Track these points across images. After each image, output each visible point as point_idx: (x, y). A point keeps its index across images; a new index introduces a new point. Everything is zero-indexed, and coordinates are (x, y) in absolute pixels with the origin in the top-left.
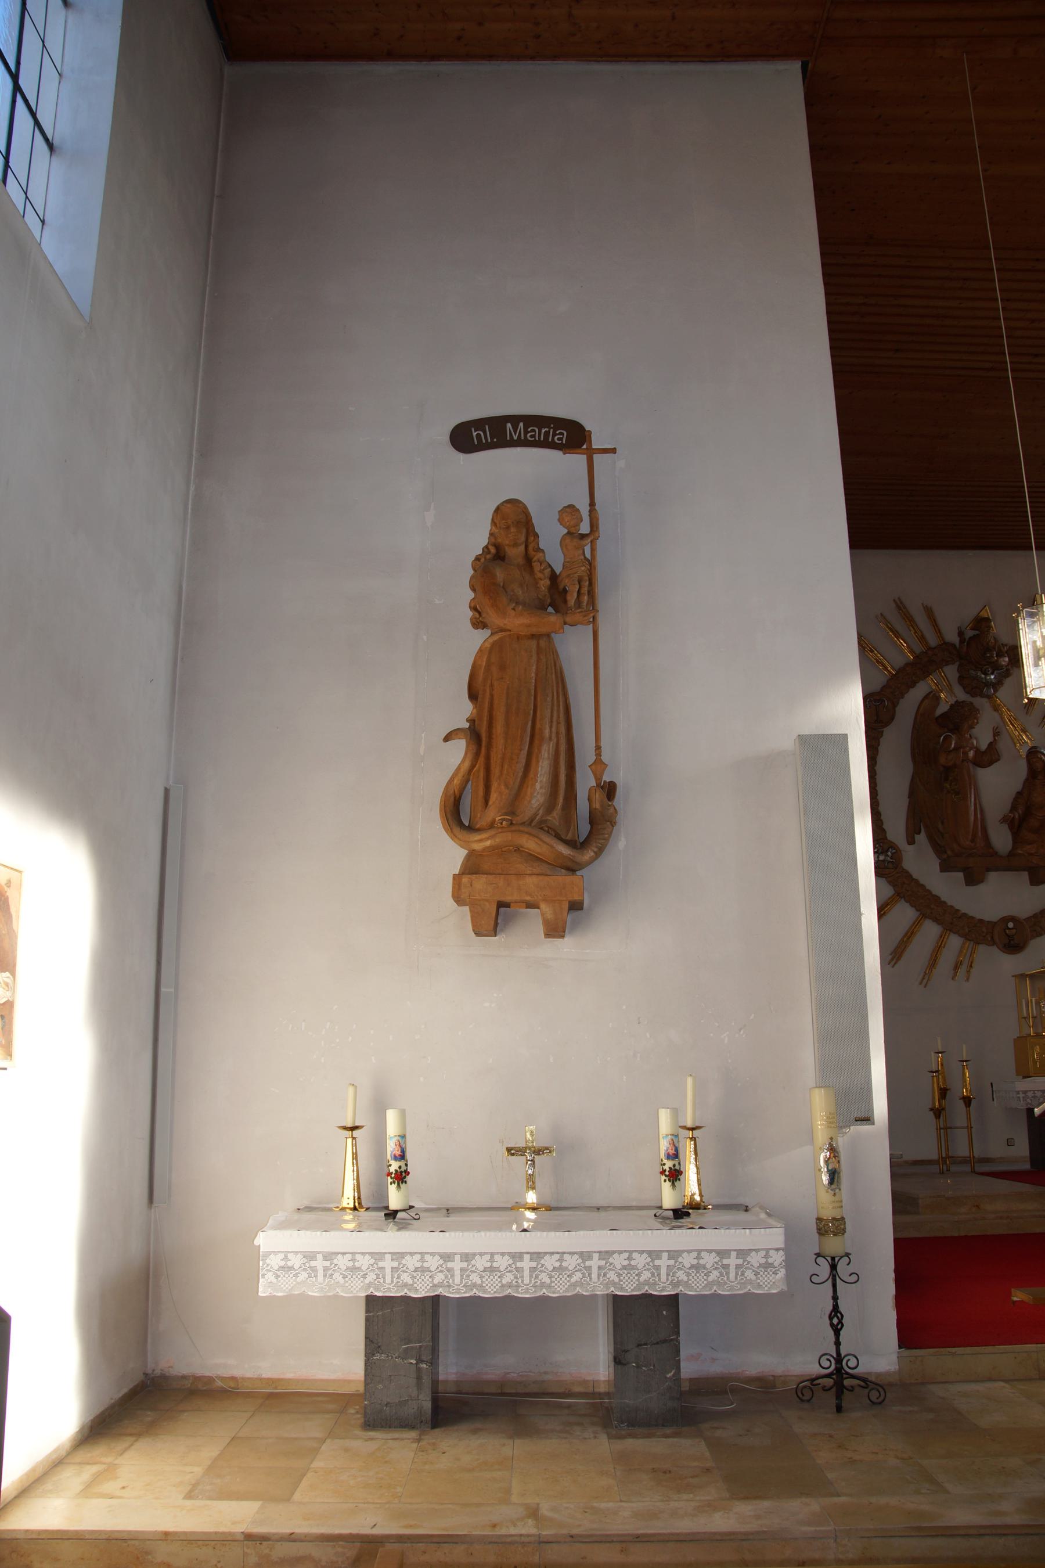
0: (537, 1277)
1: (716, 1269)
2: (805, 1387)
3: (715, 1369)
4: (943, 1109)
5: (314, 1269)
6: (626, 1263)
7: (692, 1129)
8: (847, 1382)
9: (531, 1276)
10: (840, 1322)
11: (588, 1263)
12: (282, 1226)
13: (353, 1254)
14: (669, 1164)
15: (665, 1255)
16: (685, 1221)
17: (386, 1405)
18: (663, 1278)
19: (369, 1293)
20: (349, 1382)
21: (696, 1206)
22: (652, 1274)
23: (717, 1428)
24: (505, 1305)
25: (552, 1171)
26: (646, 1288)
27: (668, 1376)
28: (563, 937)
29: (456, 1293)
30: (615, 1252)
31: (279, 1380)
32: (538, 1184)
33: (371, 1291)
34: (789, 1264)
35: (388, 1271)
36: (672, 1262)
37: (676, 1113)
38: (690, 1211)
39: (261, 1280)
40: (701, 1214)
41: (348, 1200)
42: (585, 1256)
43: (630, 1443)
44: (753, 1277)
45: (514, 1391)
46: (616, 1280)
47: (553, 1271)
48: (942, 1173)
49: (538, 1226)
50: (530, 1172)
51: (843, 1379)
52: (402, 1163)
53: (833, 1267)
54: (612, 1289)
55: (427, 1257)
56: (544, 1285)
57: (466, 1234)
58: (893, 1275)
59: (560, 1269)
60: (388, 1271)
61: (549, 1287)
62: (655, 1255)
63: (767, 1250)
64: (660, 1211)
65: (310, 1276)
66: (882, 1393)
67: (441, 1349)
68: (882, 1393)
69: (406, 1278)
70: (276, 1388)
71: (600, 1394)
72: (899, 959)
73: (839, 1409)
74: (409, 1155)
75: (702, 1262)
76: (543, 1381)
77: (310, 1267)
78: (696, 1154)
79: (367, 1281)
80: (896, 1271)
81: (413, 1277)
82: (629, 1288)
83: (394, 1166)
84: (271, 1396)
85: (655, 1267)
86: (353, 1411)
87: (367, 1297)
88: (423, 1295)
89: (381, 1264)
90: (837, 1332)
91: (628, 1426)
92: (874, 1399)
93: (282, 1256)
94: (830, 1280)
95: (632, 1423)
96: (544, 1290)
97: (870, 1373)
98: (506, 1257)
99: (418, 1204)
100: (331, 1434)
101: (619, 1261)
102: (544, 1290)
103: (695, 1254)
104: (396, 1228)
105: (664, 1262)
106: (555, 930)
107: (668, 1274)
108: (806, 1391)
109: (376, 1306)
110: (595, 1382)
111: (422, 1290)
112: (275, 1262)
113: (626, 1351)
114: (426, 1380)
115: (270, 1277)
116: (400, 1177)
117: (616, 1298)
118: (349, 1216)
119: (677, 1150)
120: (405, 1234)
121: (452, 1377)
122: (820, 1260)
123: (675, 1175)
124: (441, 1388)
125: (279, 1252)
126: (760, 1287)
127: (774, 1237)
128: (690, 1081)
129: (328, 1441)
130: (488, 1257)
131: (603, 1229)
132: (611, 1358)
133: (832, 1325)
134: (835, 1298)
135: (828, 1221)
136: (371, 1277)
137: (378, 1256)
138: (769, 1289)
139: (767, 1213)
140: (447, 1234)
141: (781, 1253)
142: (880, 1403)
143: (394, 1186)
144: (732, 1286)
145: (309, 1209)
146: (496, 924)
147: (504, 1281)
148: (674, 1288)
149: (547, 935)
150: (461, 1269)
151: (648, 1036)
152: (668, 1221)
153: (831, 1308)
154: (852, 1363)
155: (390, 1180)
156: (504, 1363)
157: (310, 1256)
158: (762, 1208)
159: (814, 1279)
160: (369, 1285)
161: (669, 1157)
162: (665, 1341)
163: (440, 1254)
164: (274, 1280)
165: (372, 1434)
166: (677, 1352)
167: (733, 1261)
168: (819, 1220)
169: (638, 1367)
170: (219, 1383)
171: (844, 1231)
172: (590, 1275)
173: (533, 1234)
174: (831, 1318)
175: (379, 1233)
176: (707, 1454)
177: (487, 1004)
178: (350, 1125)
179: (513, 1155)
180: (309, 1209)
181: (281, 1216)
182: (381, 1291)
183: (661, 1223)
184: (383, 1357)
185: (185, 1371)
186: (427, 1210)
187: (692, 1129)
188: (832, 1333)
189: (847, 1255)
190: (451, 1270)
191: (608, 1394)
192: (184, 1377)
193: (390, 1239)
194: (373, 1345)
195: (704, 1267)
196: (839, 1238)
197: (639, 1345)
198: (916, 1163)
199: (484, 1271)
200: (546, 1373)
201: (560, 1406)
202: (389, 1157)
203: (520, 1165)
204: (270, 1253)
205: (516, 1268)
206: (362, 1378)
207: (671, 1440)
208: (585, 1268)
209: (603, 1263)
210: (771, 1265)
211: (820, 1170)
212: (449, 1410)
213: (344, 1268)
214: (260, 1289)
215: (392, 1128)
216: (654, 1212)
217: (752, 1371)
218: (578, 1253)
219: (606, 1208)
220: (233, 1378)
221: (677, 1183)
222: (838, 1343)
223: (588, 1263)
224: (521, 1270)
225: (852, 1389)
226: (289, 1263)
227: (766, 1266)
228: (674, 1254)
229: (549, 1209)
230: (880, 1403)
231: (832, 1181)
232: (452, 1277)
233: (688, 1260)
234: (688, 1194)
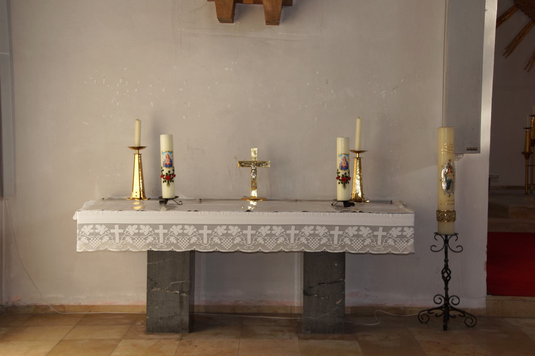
0: (256, 239)
1: (369, 237)
2: (424, 314)
3: (367, 301)
4: (532, 153)
5: (113, 234)
6: (312, 232)
7: (359, 152)
8: (452, 313)
9: (252, 239)
10: (449, 275)
11: (288, 232)
12: (91, 208)
13: (139, 225)
14: (342, 173)
16: (352, 208)
17: (161, 319)
18: (336, 242)
19: (149, 249)
20: (138, 306)
21: (359, 200)
22: (329, 239)
23: (367, 336)
24: (235, 256)
25: (268, 178)
26: (325, 248)
27: (337, 303)
28: (278, 24)
29: (204, 249)
30: (305, 225)
31: (93, 306)
32: (259, 186)
33: (151, 248)
34: (416, 236)
35: (161, 236)
37: (348, 141)
38: (355, 203)
39: (78, 242)
40: (362, 205)
41: (136, 193)
42: (286, 227)
43: (312, 342)
44: (393, 244)
45: (241, 312)
46: (306, 242)
48: (527, 194)
49: (256, 208)
50: (254, 177)
51: (449, 310)
52: (171, 169)
53: (446, 241)
54: (303, 248)
57: (211, 213)
58: (486, 249)
59: (270, 235)
60: (161, 236)
61: (263, 246)
62: (330, 227)
63: (403, 227)
64: (336, 202)
65: (110, 239)
66: (474, 321)
67: (196, 286)
68: (474, 321)
69: (173, 240)
70: (90, 311)
71: (295, 314)
72: (511, 53)
73: (445, 328)
74: (175, 164)
75: (360, 233)
76: (260, 306)
77: (111, 233)
78: (360, 168)
79: (148, 242)
80: (488, 247)
81: (177, 239)
82: (314, 247)
83: (166, 171)
84: (86, 316)
86: (139, 323)
87: (148, 251)
88: (183, 250)
90: (446, 281)
91: (311, 332)
92: (468, 324)
93: (92, 226)
94: (444, 249)
95: (314, 331)
96: (260, 248)
97: (467, 309)
98: (237, 227)
99: (181, 197)
100: (125, 337)
101: (307, 231)
102: (260, 248)
103: (356, 228)
104: (166, 209)
106: (273, 20)
107: (338, 240)
108: (425, 317)
109: (153, 256)
110: (292, 307)
111: (183, 247)
112: (87, 230)
113: (311, 287)
114: (186, 304)
115: (84, 240)
116: (170, 178)
117: (306, 254)
118: (137, 203)
119: (347, 164)
120: (172, 213)
121: (203, 303)
122: (438, 237)
123: (346, 180)
124: (196, 310)
125: (90, 224)
126: (396, 249)
127: (408, 219)
128: (358, 121)
129: (123, 341)
130: (225, 227)
131: (298, 211)
132: (302, 292)
133: (443, 277)
134: (446, 261)
135: (444, 212)
136: (150, 239)
137: (155, 226)
138: (403, 251)
139: (404, 205)
140: (199, 213)
141: (412, 229)
142: (473, 326)
143: (165, 184)
144: (379, 248)
145: (110, 199)
146: (233, 14)
147: (235, 242)
148: (342, 248)
149: (268, 22)
150: (208, 234)
151: (332, 92)
152: (340, 208)
153: (443, 267)
154: (456, 301)
155: (163, 180)
156: (236, 295)
157: (110, 226)
158: (400, 202)
159: (433, 248)
160: (149, 244)
161: (342, 168)
162: (335, 282)
163: (194, 225)
164: (87, 242)
165: (151, 336)
166: (343, 289)
167: (380, 233)
168: (439, 211)
169: (318, 297)
170: (52, 309)
171: (454, 219)
172: (289, 239)
173: (254, 213)
174: (443, 273)
175: (156, 212)
176: (360, 350)
177: (227, 69)
178: (137, 145)
179: (243, 166)
180: (110, 199)
181: (91, 202)
182: (156, 248)
183: (336, 209)
184: (159, 289)
185: (29, 303)
186: (187, 200)
187: (359, 152)
188: (444, 282)
189: (456, 234)
190: (201, 235)
191: (299, 315)
192: (28, 306)
193: (163, 216)
194: (152, 282)
195: (361, 236)
196: (451, 223)
197: (319, 284)
198: (509, 188)
199: (134, 235)
200: (262, 301)
201: (270, 321)
202: (162, 165)
203: (248, 173)
204: (83, 225)
205: (243, 234)
206: (146, 304)
207: (337, 341)
208: (286, 235)
209: (297, 232)
210: (405, 236)
211: (441, 180)
212: (199, 322)
213: (132, 233)
214: (78, 247)
215: (164, 146)
216: (332, 203)
217: (391, 304)
218: (282, 225)
219: (301, 201)
220: (62, 306)
221: (347, 185)
222: (446, 289)
223: (288, 232)
224: (332, 236)
225: (454, 317)
226: (97, 231)
227: (402, 237)
228: (343, 228)
229: (265, 200)
230: (473, 326)
231: (448, 187)
232: (202, 239)
233: (351, 232)
234: (354, 193)
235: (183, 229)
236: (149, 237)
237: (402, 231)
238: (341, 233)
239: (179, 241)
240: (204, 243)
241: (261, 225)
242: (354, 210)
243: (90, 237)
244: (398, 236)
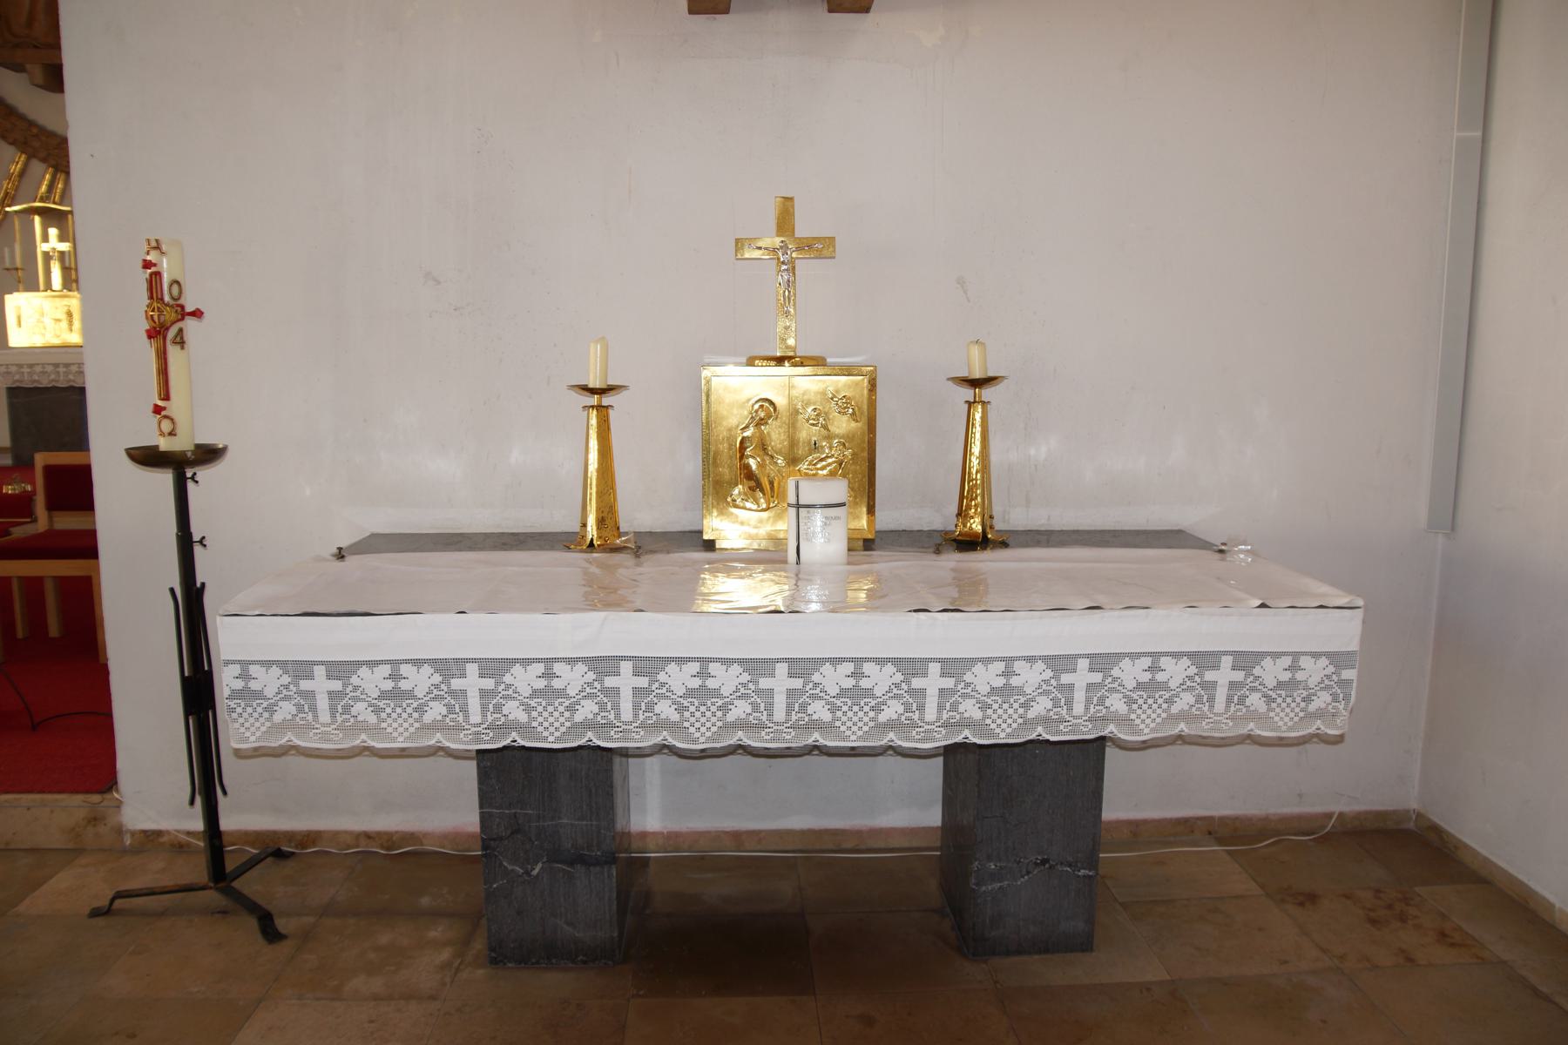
15: (1083, 664)
26: (1252, 725)
29: (1072, 732)
36: (949, 683)
55: (254, 670)
56: (1253, 716)
85: (911, 692)
96: (966, 733)
98: (581, 668)
102: (514, 735)
105: (1081, 677)
125: (690, 660)
150: (941, 691)
205: (758, 692)
209: (797, 683)
233: (1131, 673)
237: (1008, 673)
238: (949, 683)
239: (383, 715)
240: (321, 719)
241: (823, 661)
242: (1006, 605)
244: (1139, 684)
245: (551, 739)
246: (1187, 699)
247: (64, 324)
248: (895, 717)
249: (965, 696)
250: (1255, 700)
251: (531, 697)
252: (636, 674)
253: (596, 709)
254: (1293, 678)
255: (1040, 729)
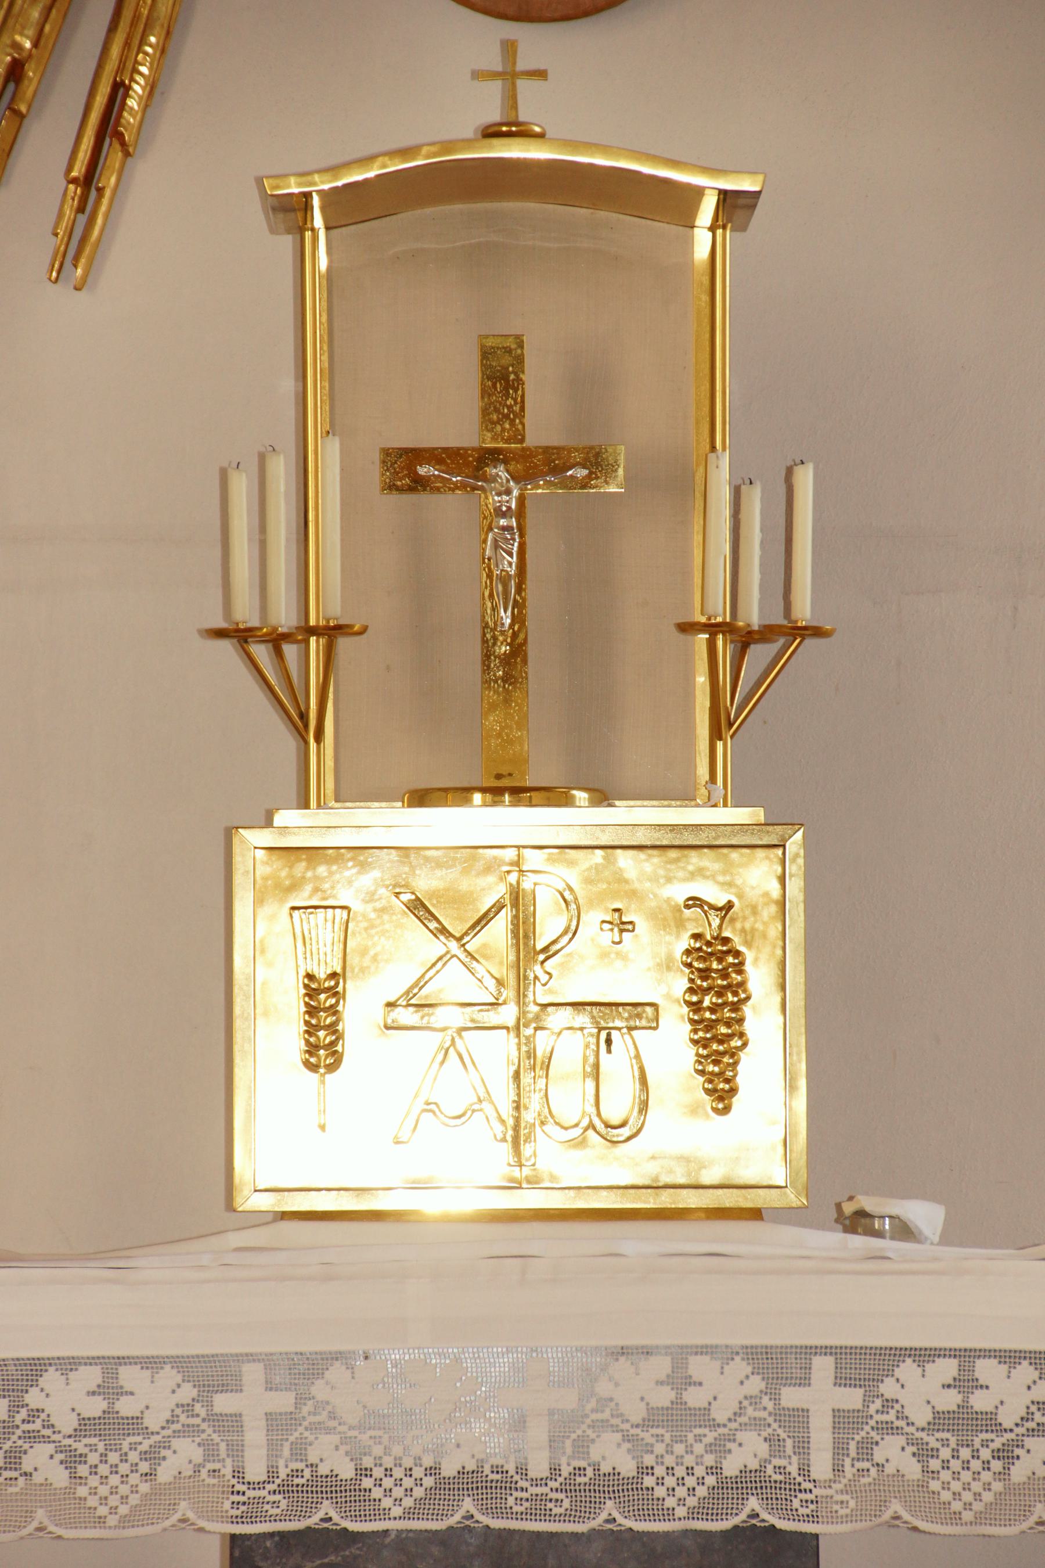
47: (77, 1434)
85: (216, 1420)
89: (223, 1403)
96: (753, 1503)
102: (327, 1508)
125: (647, 1352)
190: (798, 1419)
199: (932, 1427)
235: (966, 1383)
236: (176, 1443)
239: (935, 1464)
243: (80, 1447)
245: (681, 1512)
246: (185, 1452)
247: (671, 1048)
248: (753, 1465)
249: (32, 1437)
250: (893, 1452)
251: (361, 1427)
252: (841, 1380)
253: (763, 1449)
254: (679, 1403)
255: (468, 1505)
